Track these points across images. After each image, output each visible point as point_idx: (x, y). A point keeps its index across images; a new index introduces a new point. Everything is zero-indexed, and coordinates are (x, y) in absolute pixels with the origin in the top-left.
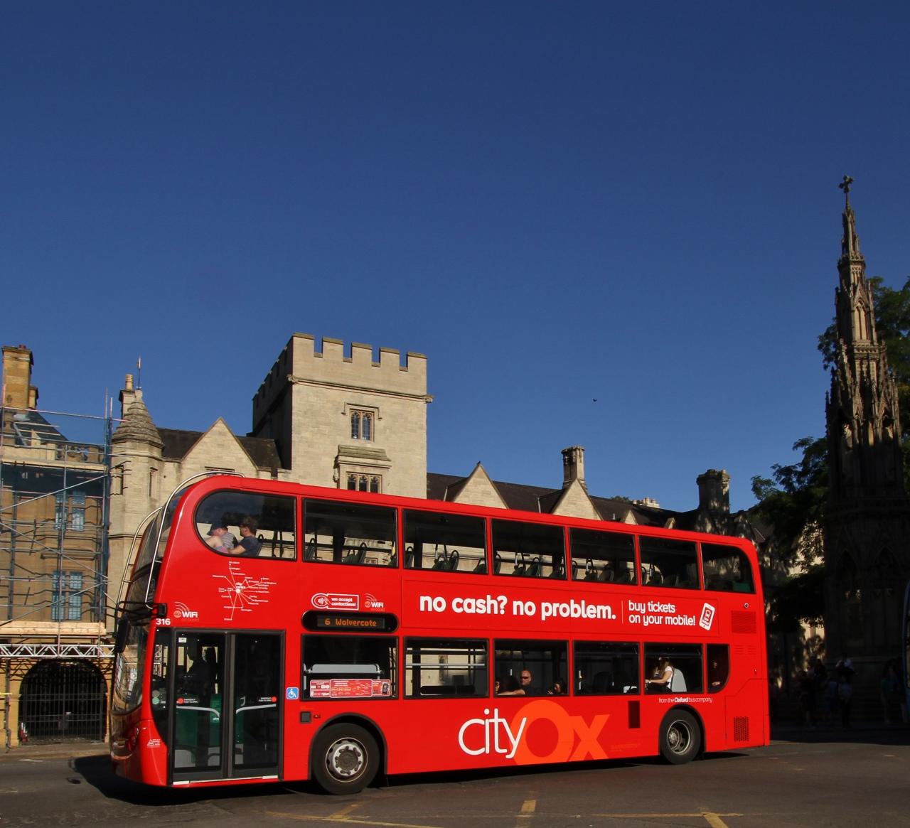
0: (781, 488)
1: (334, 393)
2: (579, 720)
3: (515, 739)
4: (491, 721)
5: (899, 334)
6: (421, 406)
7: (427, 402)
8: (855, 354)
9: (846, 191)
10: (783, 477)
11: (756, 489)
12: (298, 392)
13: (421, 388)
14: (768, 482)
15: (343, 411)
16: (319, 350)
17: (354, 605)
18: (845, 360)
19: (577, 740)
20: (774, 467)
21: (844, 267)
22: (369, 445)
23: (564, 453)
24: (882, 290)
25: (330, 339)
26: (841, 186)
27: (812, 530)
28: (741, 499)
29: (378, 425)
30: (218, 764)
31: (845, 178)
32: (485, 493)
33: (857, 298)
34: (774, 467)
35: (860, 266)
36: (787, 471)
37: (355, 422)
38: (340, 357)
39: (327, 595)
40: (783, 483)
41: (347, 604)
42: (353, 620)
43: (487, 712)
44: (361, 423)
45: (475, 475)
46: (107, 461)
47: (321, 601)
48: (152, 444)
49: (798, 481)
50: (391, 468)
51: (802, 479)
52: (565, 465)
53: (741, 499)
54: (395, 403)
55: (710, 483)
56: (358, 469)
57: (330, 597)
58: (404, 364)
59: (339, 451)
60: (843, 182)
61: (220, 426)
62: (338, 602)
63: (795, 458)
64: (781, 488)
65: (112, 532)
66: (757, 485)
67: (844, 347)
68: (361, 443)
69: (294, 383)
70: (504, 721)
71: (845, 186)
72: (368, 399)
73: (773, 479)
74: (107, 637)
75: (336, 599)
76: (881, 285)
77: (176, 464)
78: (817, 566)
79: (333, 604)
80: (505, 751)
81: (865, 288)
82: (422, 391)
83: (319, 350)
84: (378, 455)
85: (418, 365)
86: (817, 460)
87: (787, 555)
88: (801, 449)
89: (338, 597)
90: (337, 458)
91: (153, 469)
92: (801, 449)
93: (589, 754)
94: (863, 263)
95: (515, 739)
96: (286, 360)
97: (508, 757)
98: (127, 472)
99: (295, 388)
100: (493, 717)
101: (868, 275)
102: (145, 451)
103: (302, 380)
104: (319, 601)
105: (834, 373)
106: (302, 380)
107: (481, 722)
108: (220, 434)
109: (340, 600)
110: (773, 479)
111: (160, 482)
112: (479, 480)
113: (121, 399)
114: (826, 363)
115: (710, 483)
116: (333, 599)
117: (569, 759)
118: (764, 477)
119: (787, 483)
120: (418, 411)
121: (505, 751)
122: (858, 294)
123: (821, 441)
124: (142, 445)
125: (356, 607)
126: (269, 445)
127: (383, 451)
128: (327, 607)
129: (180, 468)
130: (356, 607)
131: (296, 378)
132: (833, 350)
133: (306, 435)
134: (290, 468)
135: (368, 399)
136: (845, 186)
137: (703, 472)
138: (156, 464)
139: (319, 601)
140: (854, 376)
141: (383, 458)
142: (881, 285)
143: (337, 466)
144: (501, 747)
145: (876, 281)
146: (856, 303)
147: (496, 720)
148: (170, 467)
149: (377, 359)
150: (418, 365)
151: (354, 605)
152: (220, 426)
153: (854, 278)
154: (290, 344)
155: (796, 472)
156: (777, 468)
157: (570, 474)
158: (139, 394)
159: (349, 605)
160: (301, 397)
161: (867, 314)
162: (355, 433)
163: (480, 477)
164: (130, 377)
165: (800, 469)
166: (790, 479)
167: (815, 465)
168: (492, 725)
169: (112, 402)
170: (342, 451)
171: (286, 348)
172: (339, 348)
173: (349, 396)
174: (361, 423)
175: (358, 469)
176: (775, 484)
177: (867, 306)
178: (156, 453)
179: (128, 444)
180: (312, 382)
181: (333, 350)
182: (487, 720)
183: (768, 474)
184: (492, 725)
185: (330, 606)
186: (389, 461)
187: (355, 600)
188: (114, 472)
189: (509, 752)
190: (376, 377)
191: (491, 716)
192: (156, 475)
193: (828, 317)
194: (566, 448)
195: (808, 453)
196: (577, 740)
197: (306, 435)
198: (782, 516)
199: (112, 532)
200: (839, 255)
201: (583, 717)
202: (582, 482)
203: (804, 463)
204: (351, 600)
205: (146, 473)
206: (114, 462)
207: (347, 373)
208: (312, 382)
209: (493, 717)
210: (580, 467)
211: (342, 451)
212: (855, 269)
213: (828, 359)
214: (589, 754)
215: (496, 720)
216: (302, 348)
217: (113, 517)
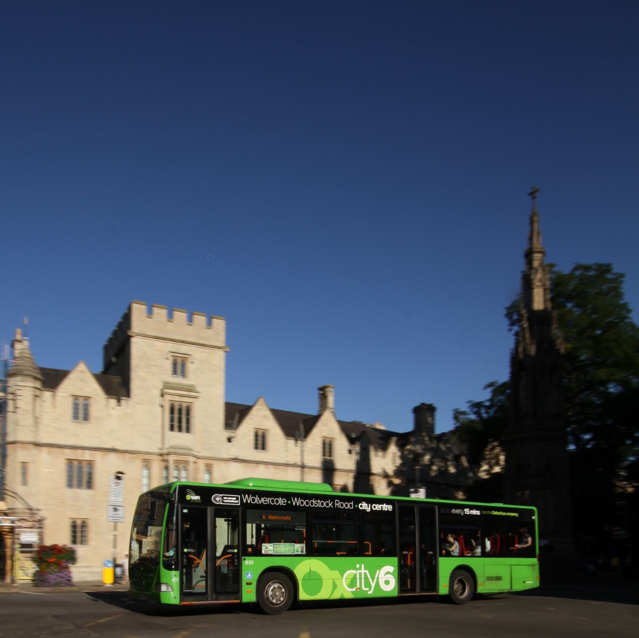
0: (473, 417)
2: (336, 574)
3: (373, 581)
4: (360, 571)
5: (565, 307)
9: (534, 198)
11: (456, 418)
13: (221, 341)
14: (464, 413)
16: (150, 313)
17: (237, 502)
19: (335, 586)
22: (184, 381)
24: (555, 272)
27: (493, 448)
28: (444, 424)
29: (190, 367)
30: (203, 590)
32: (265, 417)
33: (538, 278)
34: (468, 402)
36: (477, 406)
37: (175, 364)
39: (221, 495)
40: (475, 413)
41: (232, 501)
42: (278, 516)
43: (358, 566)
44: (179, 366)
47: (217, 499)
48: (36, 378)
53: (444, 424)
55: (424, 412)
56: (177, 398)
57: (223, 497)
58: (209, 324)
61: (82, 367)
62: (227, 500)
63: (485, 396)
64: (473, 417)
66: (457, 414)
68: (178, 380)
70: (367, 571)
72: (184, 349)
75: (226, 498)
76: (555, 269)
78: (497, 473)
79: (225, 501)
80: (368, 589)
81: (544, 270)
82: (221, 343)
83: (150, 313)
84: (191, 389)
85: (219, 324)
87: (475, 463)
88: (490, 389)
89: (228, 497)
93: (342, 594)
95: (373, 581)
96: (126, 321)
97: (369, 593)
98: (19, 397)
100: (361, 569)
101: (548, 261)
103: (139, 335)
104: (217, 499)
105: (517, 334)
106: (139, 335)
107: (354, 572)
108: (83, 372)
109: (229, 498)
110: (468, 410)
113: (12, 346)
115: (424, 412)
116: (225, 498)
117: (331, 596)
119: (477, 413)
120: (219, 358)
121: (368, 589)
123: (505, 384)
124: (27, 378)
125: (238, 503)
127: (193, 386)
128: (221, 503)
129: (54, 396)
130: (238, 503)
132: (515, 317)
133: (141, 373)
135: (184, 349)
136: (533, 194)
138: (38, 393)
139: (217, 499)
141: (193, 391)
142: (555, 269)
143: (162, 395)
144: (365, 587)
145: (552, 266)
147: (363, 571)
148: (47, 395)
150: (219, 324)
151: (237, 502)
152: (82, 367)
153: (536, 264)
154: (130, 309)
157: (323, 406)
158: (26, 343)
160: (138, 347)
162: (175, 372)
165: (487, 404)
168: (360, 574)
169: (7, 347)
173: (171, 346)
174: (179, 366)
175: (177, 398)
178: (38, 384)
179: (18, 378)
182: (358, 571)
183: (464, 407)
184: (360, 574)
185: (223, 502)
186: (197, 392)
187: (237, 499)
188: (10, 397)
189: (370, 590)
190: (190, 333)
191: (360, 568)
194: (321, 385)
196: (335, 586)
197: (141, 373)
198: (474, 436)
200: (525, 246)
201: (339, 571)
203: (491, 400)
204: (235, 499)
206: (10, 390)
207: (169, 330)
209: (361, 569)
210: (331, 400)
211: (167, 385)
212: (537, 256)
213: (512, 324)
214: (342, 594)
215: (363, 571)
216: (138, 311)
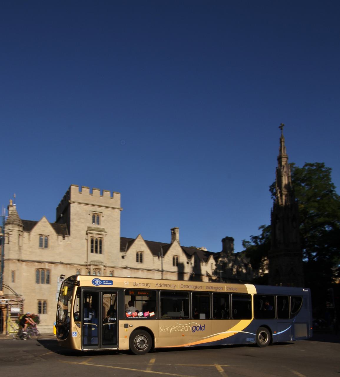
1: (86, 207)
6: (118, 212)
7: (121, 211)
8: (283, 193)
9: (282, 129)
10: (254, 240)
12: (73, 206)
14: (248, 242)
15: (89, 214)
18: (279, 195)
20: (251, 236)
21: (280, 159)
22: (99, 227)
23: (172, 230)
25: (85, 187)
26: (280, 127)
29: (102, 219)
31: (281, 124)
33: (284, 171)
34: (251, 236)
35: (286, 159)
37: (94, 218)
38: (88, 193)
40: (254, 242)
44: (96, 219)
45: (138, 238)
46: (3, 232)
48: (20, 226)
49: (260, 242)
50: (107, 236)
51: (262, 241)
52: (172, 234)
53: (238, 248)
54: (109, 211)
58: (112, 196)
59: (88, 229)
60: (280, 126)
61: (44, 219)
62: (105, 282)
65: (5, 258)
67: (279, 191)
69: (71, 203)
71: (281, 127)
72: (99, 209)
73: (250, 241)
74: (4, 296)
76: (294, 166)
77: (28, 233)
81: (287, 167)
83: (80, 191)
84: (102, 230)
85: (117, 196)
86: (267, 234)
88: (262, 229)
90: (87, 231)
91: (20, 235)
92: (262, 229)
94: (287, 158)
99: (72, 205)
102: (17, 228)
104: (96, 282)
108: (45, 222)
110: (250, 241)
111: (22, 240)
112: (139, 240)
113: (8, 209)
114: (272, 196)
118: (247, 240)
122: (285, 170)
123: (269, 226)
126: (62, 226)
127: (104, 229)
129: (29, 235)
131: (72, 201)
134: (69, 234)
135: (99, 209)
136: (281, 127)
137: (224, 237)
138: (21, 233)
140: (282, 201)
142: (294, 166)
145: (292, 164)
146: (284, 173)
148: (26, 234)
149: (102, 194)
152: (44, 219)
154: (70, 188)
155: (259, 238)
156: (252, 237)
158: (15, 207)
159: (107, 283)
160: (74, 208)
161: (288, 177)
162: (94, 221)
163: (140, 239)
164: (11, 201)
165: (260, 237)
166: (257, 241)
167: (267, 235)
170: (89, 229)
171: (68, 190)
172: (88, 190)
173: (92, 208)
174: (96, 219)
176: (251, 243)
177: (288, 174)
178: (21, 229)
179: (11, 226)
180: (78, 203)
181: (85, 191)
183: (248, 239)
188: (6, 235)
192: (21, 237)
193: (273, 179)
194: (172, 228)
195: (264, 231)
199: (5, 258)
200: (278, 154)
202: (178, 241)
203: (262, 235)
205: (17, 236)
206: (6, 232)
207: (91, 199)
208: (78, 203)
210: (178, 235)
211: (89, 229)
216: (74, 190)
217: (6, 252)
